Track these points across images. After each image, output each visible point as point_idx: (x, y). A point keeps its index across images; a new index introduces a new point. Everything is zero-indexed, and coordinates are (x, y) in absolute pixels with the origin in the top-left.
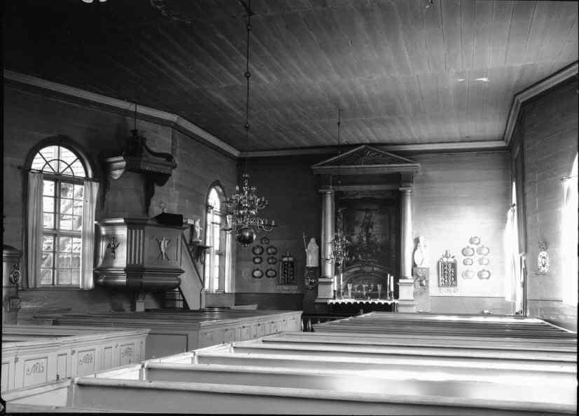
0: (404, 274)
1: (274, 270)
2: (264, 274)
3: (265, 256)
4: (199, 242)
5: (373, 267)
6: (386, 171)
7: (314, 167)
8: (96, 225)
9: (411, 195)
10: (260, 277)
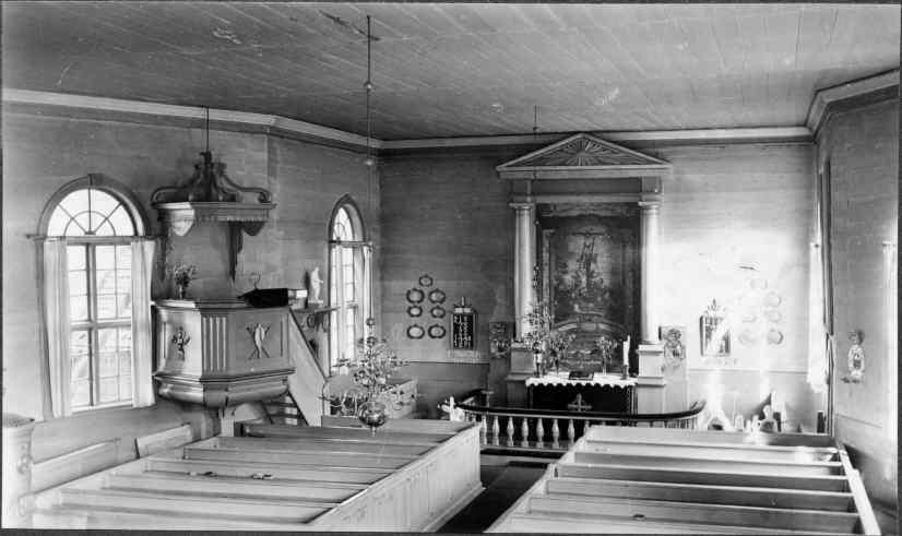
0: (647, 336)
1: (442, 328)
2: (426, 333)
3: (426, 305)
4: (318, 305)
5: (597, 323)
6: (617, 175)
7: (502, 168)
8: (152, 307)
9: (658, 214)
10: (420, 337)
